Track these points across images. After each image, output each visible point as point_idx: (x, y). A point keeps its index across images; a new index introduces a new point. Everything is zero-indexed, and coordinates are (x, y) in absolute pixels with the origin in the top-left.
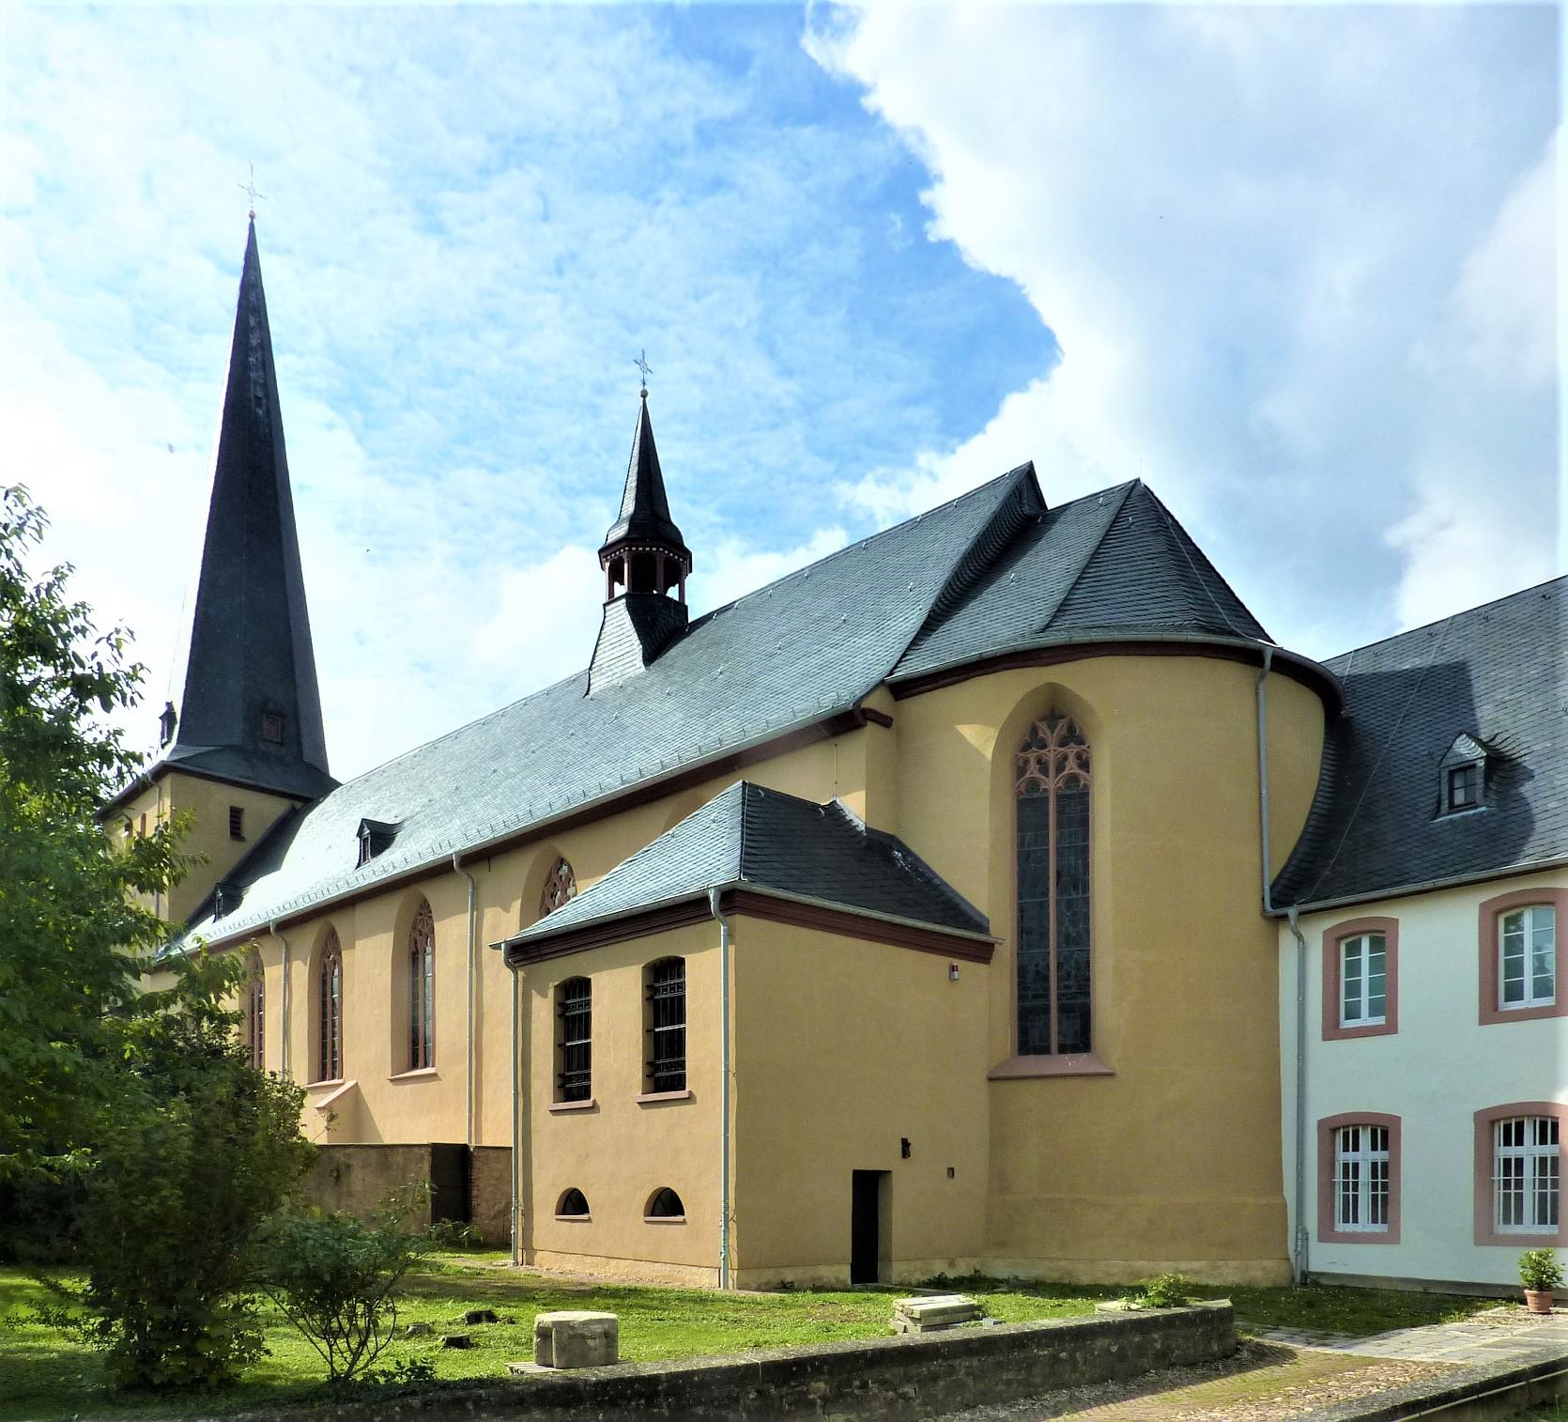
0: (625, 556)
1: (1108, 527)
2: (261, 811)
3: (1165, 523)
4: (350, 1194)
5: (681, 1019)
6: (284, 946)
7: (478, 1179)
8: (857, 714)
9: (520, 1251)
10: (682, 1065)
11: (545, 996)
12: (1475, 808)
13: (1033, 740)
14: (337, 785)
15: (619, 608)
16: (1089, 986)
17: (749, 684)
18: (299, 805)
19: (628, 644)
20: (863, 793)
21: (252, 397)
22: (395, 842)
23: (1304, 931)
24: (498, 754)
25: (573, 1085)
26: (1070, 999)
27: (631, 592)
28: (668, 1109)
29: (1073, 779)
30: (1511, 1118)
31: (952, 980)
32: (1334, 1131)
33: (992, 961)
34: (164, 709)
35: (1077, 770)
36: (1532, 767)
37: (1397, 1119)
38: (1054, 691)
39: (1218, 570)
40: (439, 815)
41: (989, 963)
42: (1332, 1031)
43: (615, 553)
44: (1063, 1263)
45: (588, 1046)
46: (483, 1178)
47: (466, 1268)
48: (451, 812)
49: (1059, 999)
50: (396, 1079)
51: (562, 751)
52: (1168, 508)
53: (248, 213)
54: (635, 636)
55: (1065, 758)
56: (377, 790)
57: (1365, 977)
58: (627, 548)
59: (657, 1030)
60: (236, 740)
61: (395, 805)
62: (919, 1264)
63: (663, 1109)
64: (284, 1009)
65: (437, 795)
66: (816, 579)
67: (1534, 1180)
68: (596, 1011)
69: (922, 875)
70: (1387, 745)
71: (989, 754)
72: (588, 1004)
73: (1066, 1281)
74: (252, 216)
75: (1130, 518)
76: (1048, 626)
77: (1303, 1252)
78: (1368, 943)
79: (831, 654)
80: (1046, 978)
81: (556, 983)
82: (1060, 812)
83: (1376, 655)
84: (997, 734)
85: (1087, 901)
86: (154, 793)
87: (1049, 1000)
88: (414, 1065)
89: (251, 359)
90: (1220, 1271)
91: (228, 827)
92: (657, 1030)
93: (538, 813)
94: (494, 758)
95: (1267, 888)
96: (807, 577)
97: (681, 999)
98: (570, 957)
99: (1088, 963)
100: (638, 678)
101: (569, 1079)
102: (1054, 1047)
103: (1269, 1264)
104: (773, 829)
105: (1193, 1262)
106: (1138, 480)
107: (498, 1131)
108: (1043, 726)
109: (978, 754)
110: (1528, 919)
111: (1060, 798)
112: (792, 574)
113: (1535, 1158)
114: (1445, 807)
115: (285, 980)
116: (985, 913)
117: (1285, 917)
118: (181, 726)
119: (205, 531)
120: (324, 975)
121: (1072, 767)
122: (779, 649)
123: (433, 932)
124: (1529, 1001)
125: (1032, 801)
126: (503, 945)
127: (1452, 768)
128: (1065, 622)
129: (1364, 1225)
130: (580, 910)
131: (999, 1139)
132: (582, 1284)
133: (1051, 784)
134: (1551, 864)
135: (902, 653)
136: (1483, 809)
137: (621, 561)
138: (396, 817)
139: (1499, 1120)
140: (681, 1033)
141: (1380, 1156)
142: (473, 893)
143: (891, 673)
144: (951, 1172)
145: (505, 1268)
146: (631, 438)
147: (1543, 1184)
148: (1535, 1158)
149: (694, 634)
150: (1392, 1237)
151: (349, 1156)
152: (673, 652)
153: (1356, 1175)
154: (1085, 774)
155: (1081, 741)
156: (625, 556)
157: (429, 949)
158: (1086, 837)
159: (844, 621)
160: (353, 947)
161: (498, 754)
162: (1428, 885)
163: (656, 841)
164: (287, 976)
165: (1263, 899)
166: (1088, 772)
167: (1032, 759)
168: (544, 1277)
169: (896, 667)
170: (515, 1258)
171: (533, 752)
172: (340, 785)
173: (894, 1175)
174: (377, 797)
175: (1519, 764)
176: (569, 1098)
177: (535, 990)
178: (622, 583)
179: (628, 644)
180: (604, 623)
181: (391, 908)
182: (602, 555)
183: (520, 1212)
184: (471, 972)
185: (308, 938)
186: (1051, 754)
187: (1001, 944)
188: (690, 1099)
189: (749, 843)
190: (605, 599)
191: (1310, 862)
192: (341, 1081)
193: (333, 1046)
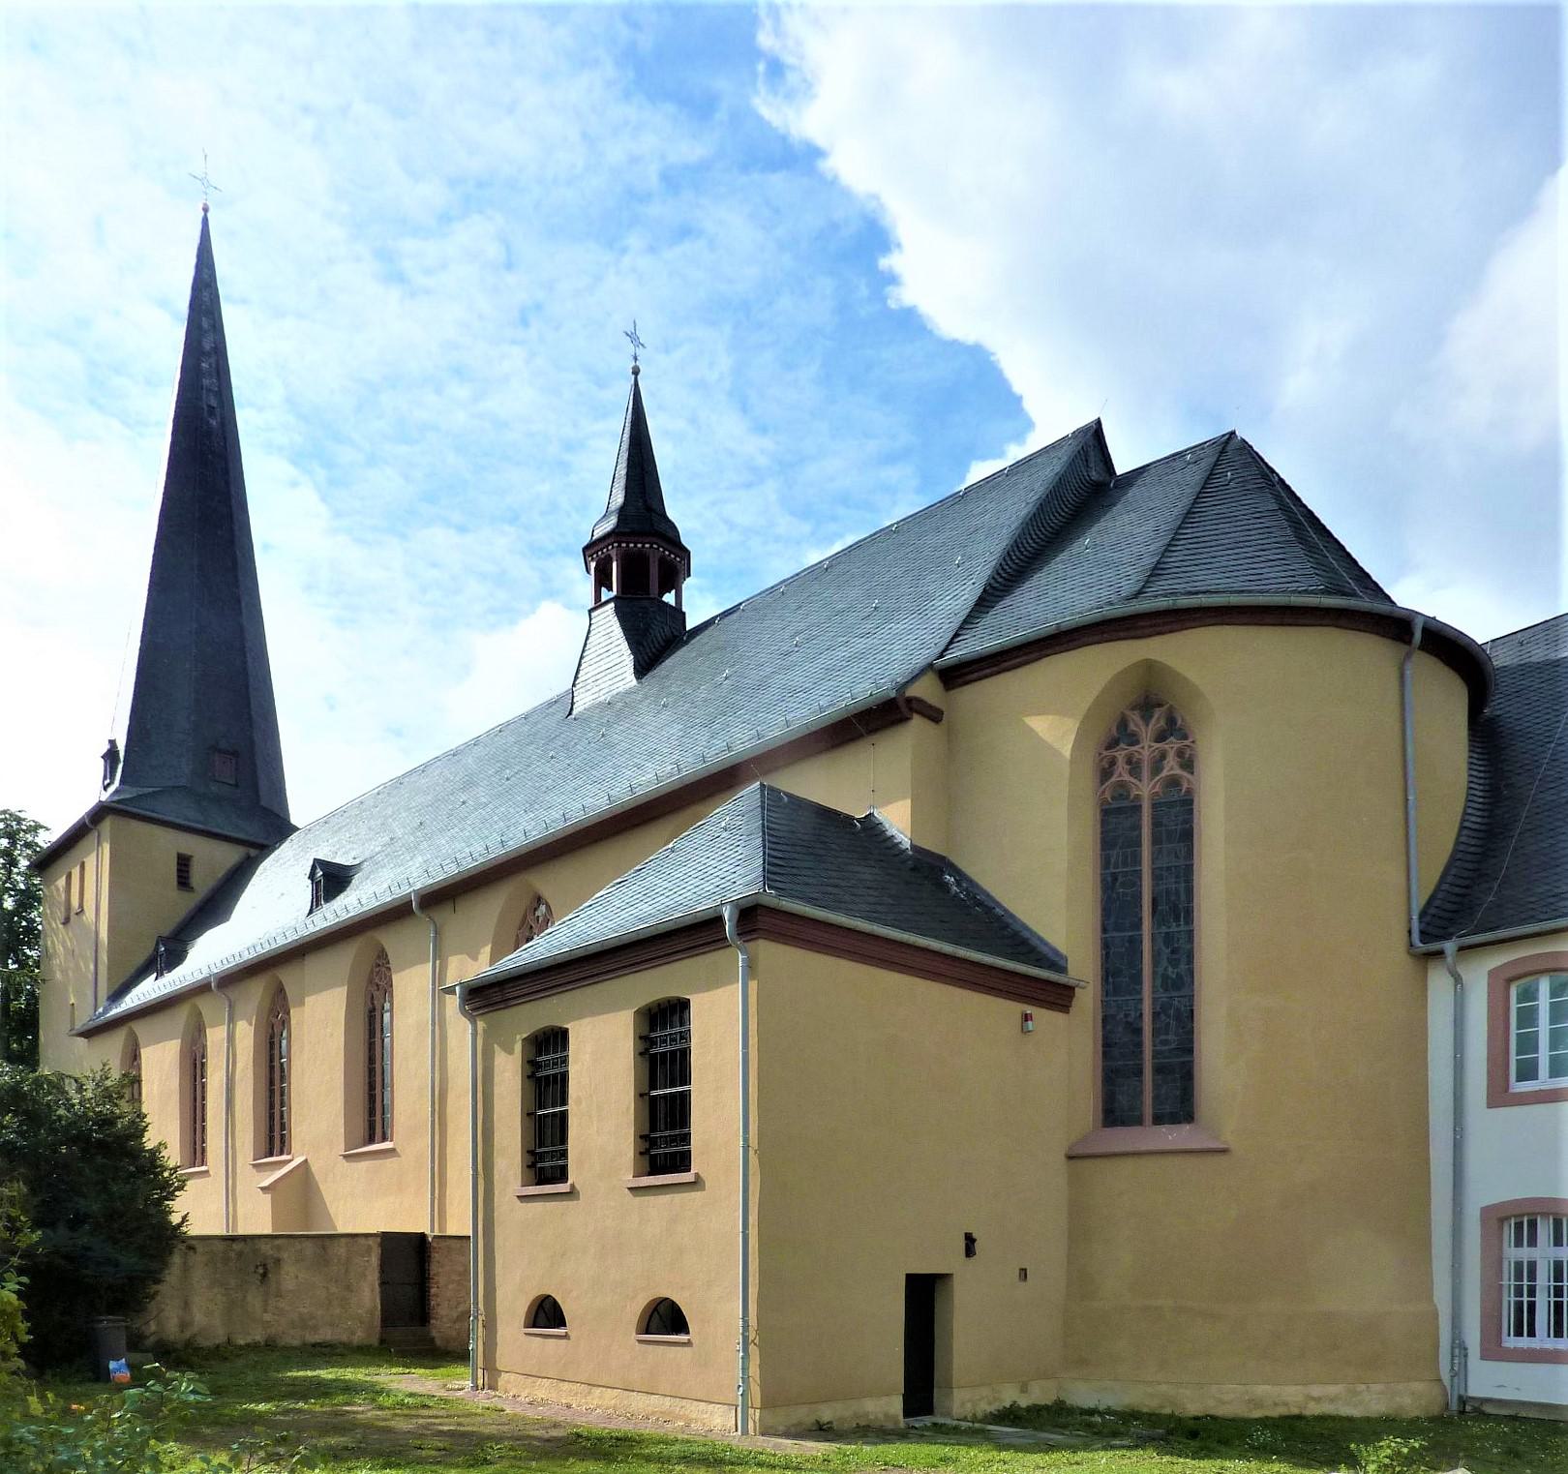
0: (613, 553)
1: (1198, 489)
2: (212, 858)
3: (1271, 481)
4: (279, 1295)
5: (685, 1079)
6: (227, 1003)
7: (437, 1274)
8: (902, 703)
9: (480, 1372)
10: (686, 1138)
11: (510, 1052)
13: (1122, 735)
14: (295, 829)
15: (607, 614)
17: (762, 685)
18: (253, 852)
19: (618, 654)
20: (908, 802)
21: (205, 407)
22: (351, 885)
23: (1461, 970)
24: (469, 784)
25: (547, 1164)
26: (1169, 1058)
27: (623, 593)
28: (668, 1196)
29: (1174, 782)
31: (1024, 1031)
32: (1502, 1220)
33: (1072, 1010)
34: (106, 747)
35: (1178, 771)
38: (1149, 667)
39: (1336, 536)
40: (400, 852)
41: (1067, 1012)
42: (1499, 1096)
43: (602, 550)
44: (1164, 1388)
45: (564, 1116)
46: (441, 1271)
47: (411, 1395)
48: (413, 849)
49: (1154, 1057)
50: (260, 1164)
51: (541, 776)
52: (1270, 464)
53: (201, 206)
54: (625, 646)
55: (1163, 756)
56: (336, 832)
57: (1544, 1027)
58: (616, 545)
59: (654, 1093)
60: (183, 782)
61: (355, 846)
62: (985, 1391)
63: (661, 1197)
64: (227, 1076)
65: (399, 833)
66: (837, 570)
68: (574, 1070)
69: (980, 904)
70: (1553, 745)
71: (1067, 751)
72: (565, 1061)
73: (1167, 1411)
74: (206, 210)
75: (1229, 474)
76: (1140, 592)
77: (1460, 1372)
79: (860, 644)
80: (1139, 1031)
81: (525, 1036)
82: (1156, 824)
83: (1521, 644)
84: (1077, 725)
85: (1190, 934)
86: (93, 837)
87: (1142, 1059)
88: (371, 1140)
89: (204, 365)
90: (1359, 1398)
91: (176, 874)
92: (654, 1093)
93: (511, 843)
94: (463, 789)
95: (1415, 917)
96: (827, 569)
97: (685, 1054)
98: (544, 1001)
100: (628, 692)
101: (541, 1157)
102: (1148, 1111)
103: (1418, 1386)
104: (800, 839)
105: (1327, 1386)
106: (1233, 433)
107: (460, 1222)
108: (1135, 717)
109: (1057, 754)
110: (1544, 986)
111: (1155, 806)
112: (808, 568)
115: (228, 1042)
116: (1062, 949)
117: (1440, 953)
118: (124, 765)
119: (152, 552)
120: (272, 1037)
121: (1171, 767)
122: (796, 646)
123: (391, 986)
125: (1119, 811)
126: (457, 988)
128: (1162, 584)
130: (555, 943)
131: (1080, 1228)
132: (555, 1426)
133: (1146, 789)
135: (953, 633)
137: (608, 560)
138: (355, 858)
140: (685, 1097)
142: (435, 937)
143: (941, 656)
144: (1024, 1274)
145: (461, 1393)
146: (618, 425)
149: (693, 642)
151: (279, 1248)
152: (668, 662)
153: (1532, 1276)
154: (1189, 776)
156: (613, 553)
157: (387, 1006)
158: (1190, 853)
159: (875, 608)
160: (302, 1003)
161: (469, 784)
163: (651, 858)
164: (231, 1038)
165: (1410, 932)
166: (1192, 773)
168: (508, 1411)
169: (946, 649)
170: (475, 1379)
171: (508, 779)
172: (298, 829)
173: (956, 1281)
174: (336, 839)
176: (541, 1181)
177: (497, 1044)
178: (610, 589)
179: (618, 654)
180: (589, 632)
181: (344, 959)
182: (587, 553)
183: (480, 1322)
184: (433, 1031)
185: (256, 992)
186: (1146, 749)
187: (1084, 988)
188: (697, 1184)
189: (772, 852)
190: (592, 604)
191: (1466, 887)
192: (289, 1157)
193: (282, 1117)
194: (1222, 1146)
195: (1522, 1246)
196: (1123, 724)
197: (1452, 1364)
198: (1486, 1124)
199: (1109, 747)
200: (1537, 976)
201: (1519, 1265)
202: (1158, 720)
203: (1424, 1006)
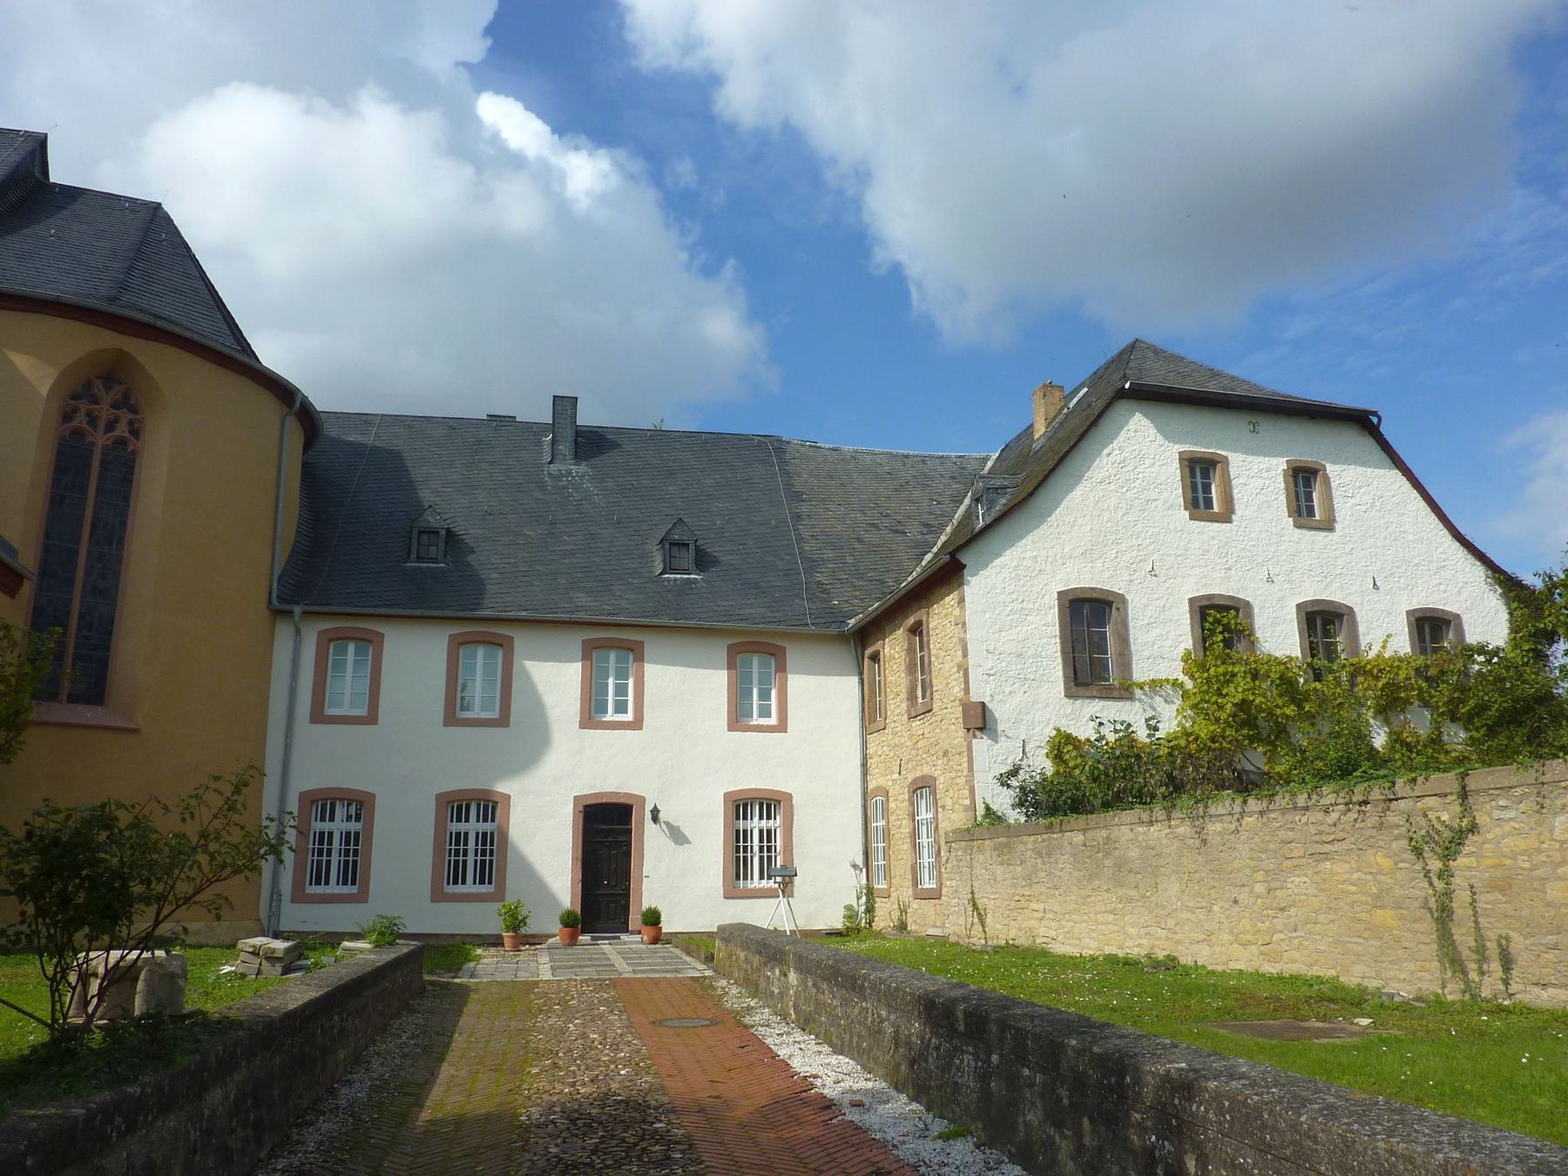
12: (437, 563)
16: (109, 640)
23: (304, 631)
30: (463, 800)
36: (473, 545)
37: (727, 795)
38: (121, 357)
55: (116, 420)
67: (341, 849)
78: (353, 650)
99: (112, 621)
113: (342, 833)
114: (414, 556)
121: (122, 430)
124: (610, 716)
127: (422, 530)
133: (100, 439)
134: (506, 617)
136: (442, 565)
139: (318, 801)
141: (353, 826)
147: (347, 853)
148: (342, 833)
150: (362, 897)
155: (133, 410)
162: (417, 612)
165: (270, 594)
166: (138, 440)
167: (82, 410)
175: (462, 540)
186: (104, 412)
194: (134, 727)
195: (461, 822)
196: (88, 385)
197: (271, 906)
198: (308, 734)
199: (74, 398)
200: (346, 641)
201: (458, 834)
202: (116, 392)
203: (271, 648)
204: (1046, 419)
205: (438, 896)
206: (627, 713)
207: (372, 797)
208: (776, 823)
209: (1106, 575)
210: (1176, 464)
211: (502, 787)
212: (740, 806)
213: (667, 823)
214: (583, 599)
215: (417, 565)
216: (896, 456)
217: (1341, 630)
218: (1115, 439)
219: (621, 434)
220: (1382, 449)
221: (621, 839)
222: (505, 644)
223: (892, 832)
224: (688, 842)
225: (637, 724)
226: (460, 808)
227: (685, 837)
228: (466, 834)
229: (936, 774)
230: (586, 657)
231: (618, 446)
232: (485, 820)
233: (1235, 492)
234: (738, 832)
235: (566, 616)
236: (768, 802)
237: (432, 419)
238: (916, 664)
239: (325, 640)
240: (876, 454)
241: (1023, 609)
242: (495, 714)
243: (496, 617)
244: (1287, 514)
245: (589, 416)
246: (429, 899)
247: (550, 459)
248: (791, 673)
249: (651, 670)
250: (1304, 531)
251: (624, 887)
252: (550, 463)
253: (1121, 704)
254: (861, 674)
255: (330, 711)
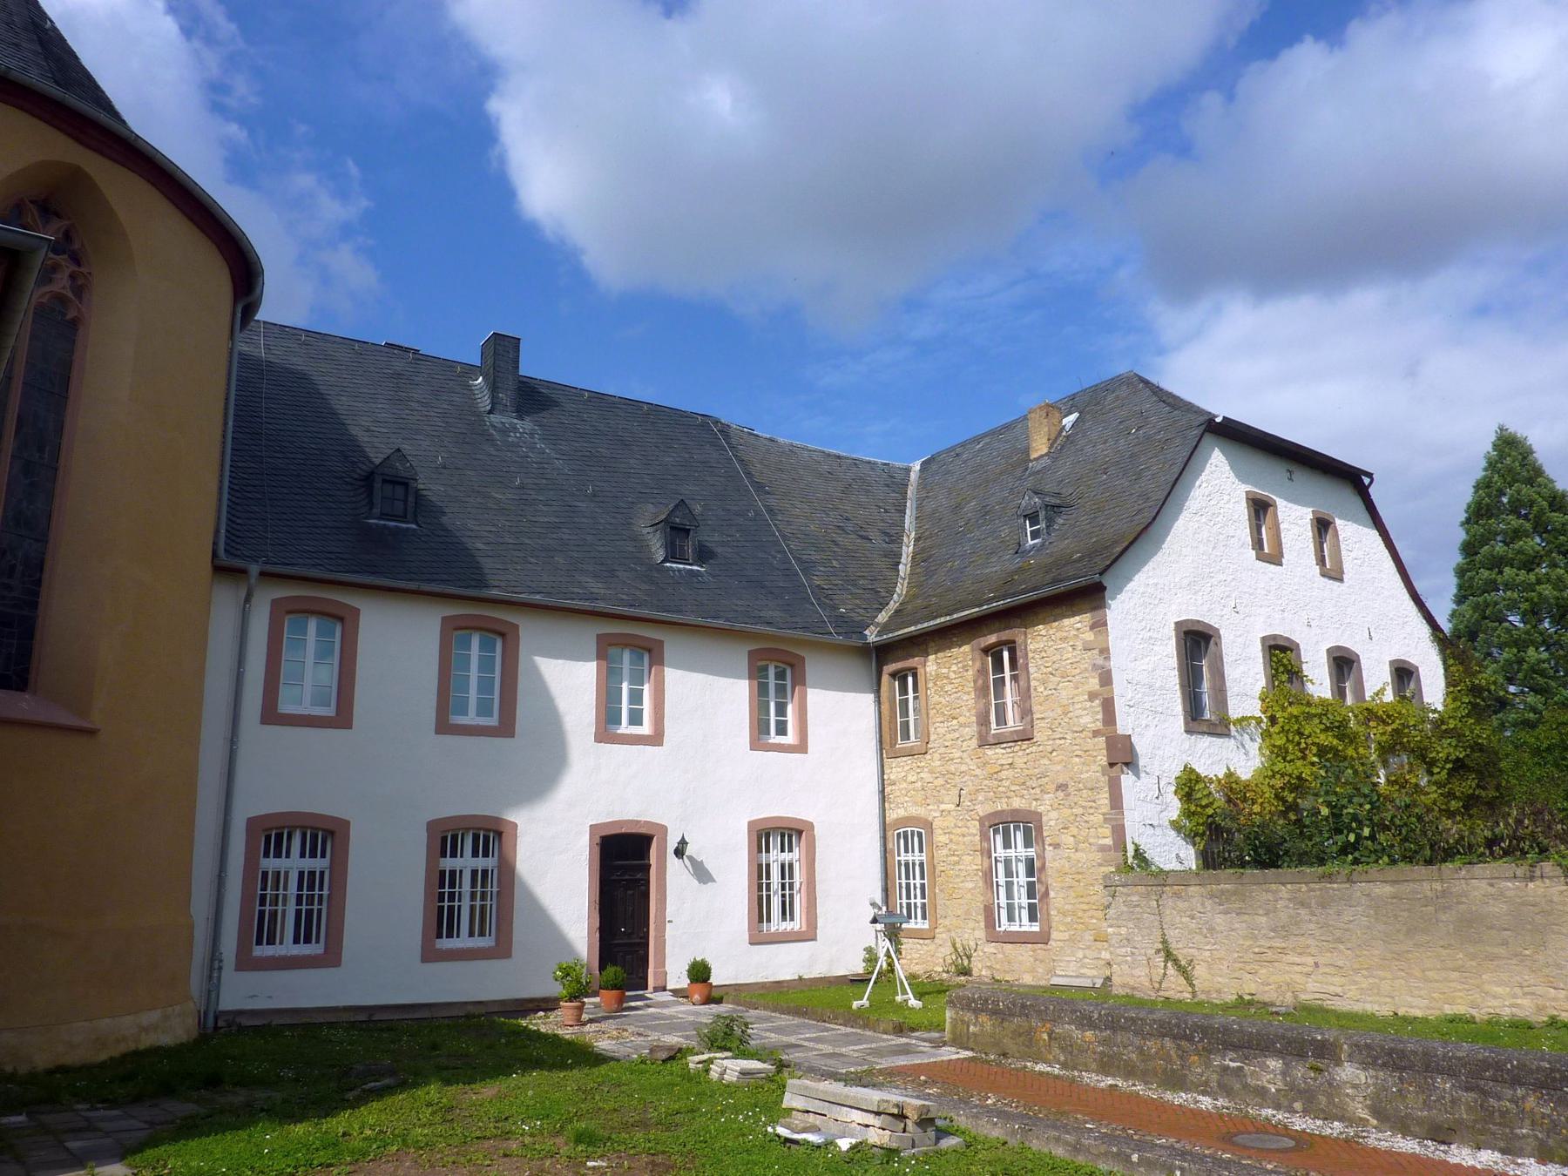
16: (37, 594)
29: (60, 299)
37: (751, 824)
38: (76, 178)
55: (55, 268)
99: (40, 567)
117: (243, 572)
121: (61, 283)
127: (388, 478)
129: (287, 948)
150: (331, 958)
162: (412, 586)
204: (1049, 440)
205: (430, 955)
206: (492, 716)
207: (345, 825)
208: (794, 856)
209: (1205, 608)
210: (1244, 504)
211: (512, 816)
212: (765, 835)
213: (690, 858)
214: (597, 587)
215: (382, 522)
216: (829, 455)
217: (1349, 675)
218: (1203, 471)
219: (554, 389)
220: (1367, 509)
221: (638, 876)
222: (506, 635)
223: (939, 868)
224: (714, 881)
225: (656, 739)
226: (279, 837)
227: (713, 878)
228: (303, 855)
229: (1041, 809)
230: (601, 655)
231: (556, 403)
232: (313, 855)
233: (1282, 536)
234: (760, 866)
235: (586, 605)
236: (790, 832)
237: (326, 337)
238: (988, 687)
239: (280, 611)
240: (810, 451)
241: (1151, 638)
242: (493, 721)
243: (501, 598)
244: (1315, 562)
245: (531, 366)
246: (418, 958)
247: (489, 408)
248: (811, 687)
249: (672, 675)
250: (1326, 580)
251: (642, 935)
252: (490, 412)
253: (1222, 740)
254: (878, 692)
255: (285, 707)
